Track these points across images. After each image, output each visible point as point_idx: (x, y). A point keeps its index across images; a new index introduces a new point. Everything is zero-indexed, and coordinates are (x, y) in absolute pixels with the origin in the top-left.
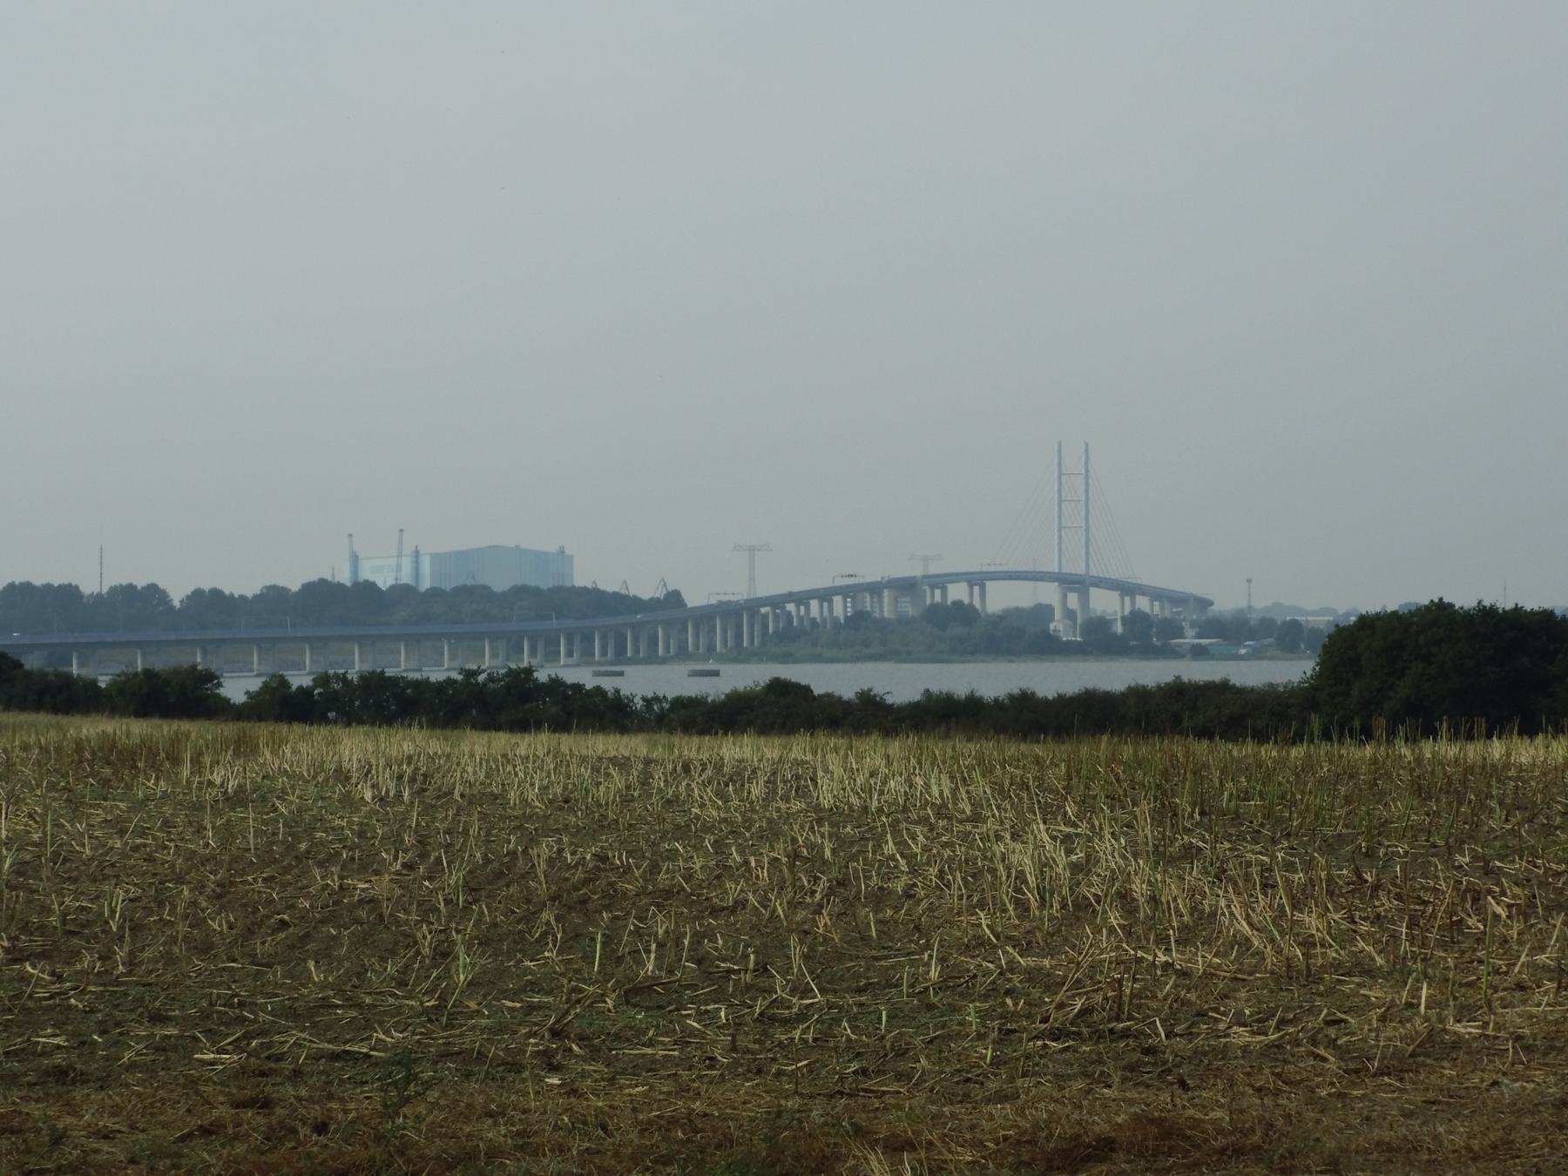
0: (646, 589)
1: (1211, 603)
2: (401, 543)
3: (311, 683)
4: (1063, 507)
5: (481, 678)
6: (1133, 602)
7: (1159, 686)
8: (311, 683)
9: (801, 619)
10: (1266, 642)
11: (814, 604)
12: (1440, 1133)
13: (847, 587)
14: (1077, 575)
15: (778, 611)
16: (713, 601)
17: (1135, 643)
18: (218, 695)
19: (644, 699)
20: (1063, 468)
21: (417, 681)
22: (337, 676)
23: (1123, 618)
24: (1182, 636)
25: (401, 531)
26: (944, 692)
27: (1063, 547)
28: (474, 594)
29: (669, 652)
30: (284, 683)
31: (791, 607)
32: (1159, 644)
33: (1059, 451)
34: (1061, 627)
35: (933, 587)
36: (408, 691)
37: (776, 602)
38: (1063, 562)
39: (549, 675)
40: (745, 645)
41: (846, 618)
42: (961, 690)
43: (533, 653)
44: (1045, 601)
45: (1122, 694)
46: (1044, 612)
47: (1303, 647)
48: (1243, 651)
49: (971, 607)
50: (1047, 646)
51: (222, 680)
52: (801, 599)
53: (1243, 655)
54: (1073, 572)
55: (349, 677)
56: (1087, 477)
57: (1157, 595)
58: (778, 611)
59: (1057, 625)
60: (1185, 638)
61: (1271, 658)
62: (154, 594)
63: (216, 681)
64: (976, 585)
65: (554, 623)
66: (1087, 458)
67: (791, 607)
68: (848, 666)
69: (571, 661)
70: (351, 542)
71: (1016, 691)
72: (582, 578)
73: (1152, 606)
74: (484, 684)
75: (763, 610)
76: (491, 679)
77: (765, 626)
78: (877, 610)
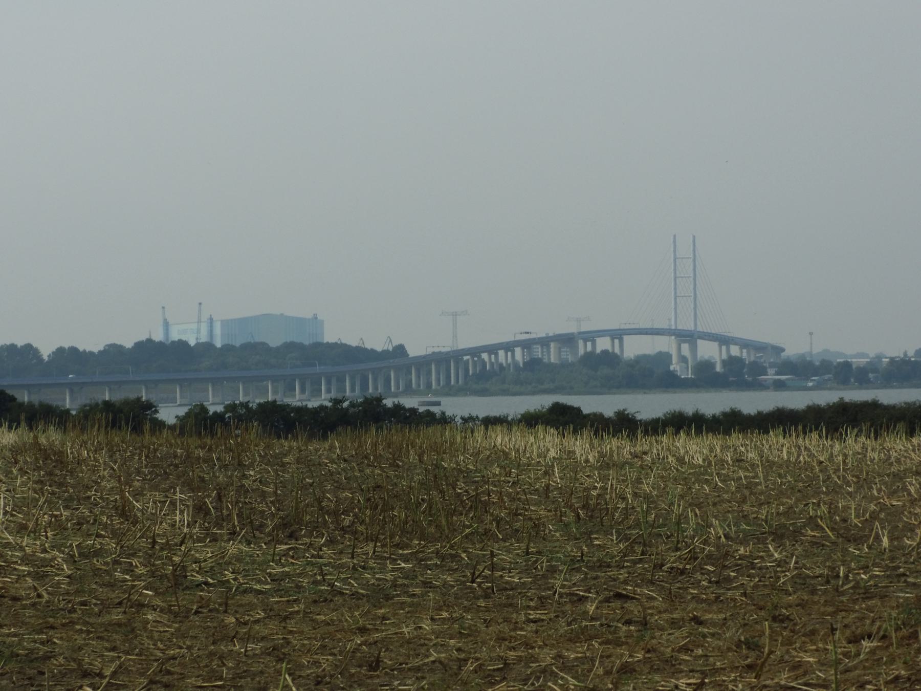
0: (377, 344)
1: (783, 350)
2: (200, 311)
3: (223, 410)
5: (346, 404)
6: (728, 350)
7: (828, 405)
8: (223, 410)
9: (492, 364)
10: (826, 377)
11: (501, 353)
13: (524, 341)
14: (688, 330)
15: (476, 359)
16: (430, 351)
17: (734, 379)
18: (157, 419)
19: (462, 418)
20: (677, 254)
21: (299, 407)
22: (241, 404)
24: (766, 374)
25: (200, 304)
26: (677, 411)
27: (678, 311)
28: (254, 349)
29: (398, 388)
30: (203, 409)
31: (485, 356)
32: (750, 379)
33: (675, 242)
34: (678, 368)
35: (585, 341)
36: (292, 415)
37: (475, 352)
39: (394, 402)
40: (452, 383)
41: (524, 363)
42: (689, 410)
43: (303, 391)
44: (664, 349)
45: (803, 411)
46: (663, 358)
47: (852, 380)
48: (810, 384)
49: (614, 354)
50: (671, 382)
51: (158, 408)
52: (492, 350)
55: (251, 405)
56: (694, 261)
57: (745, 344)
58: (476, 359)
59: (675, 366)
60: (768, 375)
61: (830, 389)
62: (29, 349)
63: (153, 409)
64: (616, 338)
65: (318, 369)
67: (485, 356)
68: (528, 397)
70: (164, 313)
71: (728, 410)
72: (330, 336)
73: (742, 352)
74: (347, 409)
75: (465, 358)
76: (352, 405)
77: (467, 370)
78: (546, 357)
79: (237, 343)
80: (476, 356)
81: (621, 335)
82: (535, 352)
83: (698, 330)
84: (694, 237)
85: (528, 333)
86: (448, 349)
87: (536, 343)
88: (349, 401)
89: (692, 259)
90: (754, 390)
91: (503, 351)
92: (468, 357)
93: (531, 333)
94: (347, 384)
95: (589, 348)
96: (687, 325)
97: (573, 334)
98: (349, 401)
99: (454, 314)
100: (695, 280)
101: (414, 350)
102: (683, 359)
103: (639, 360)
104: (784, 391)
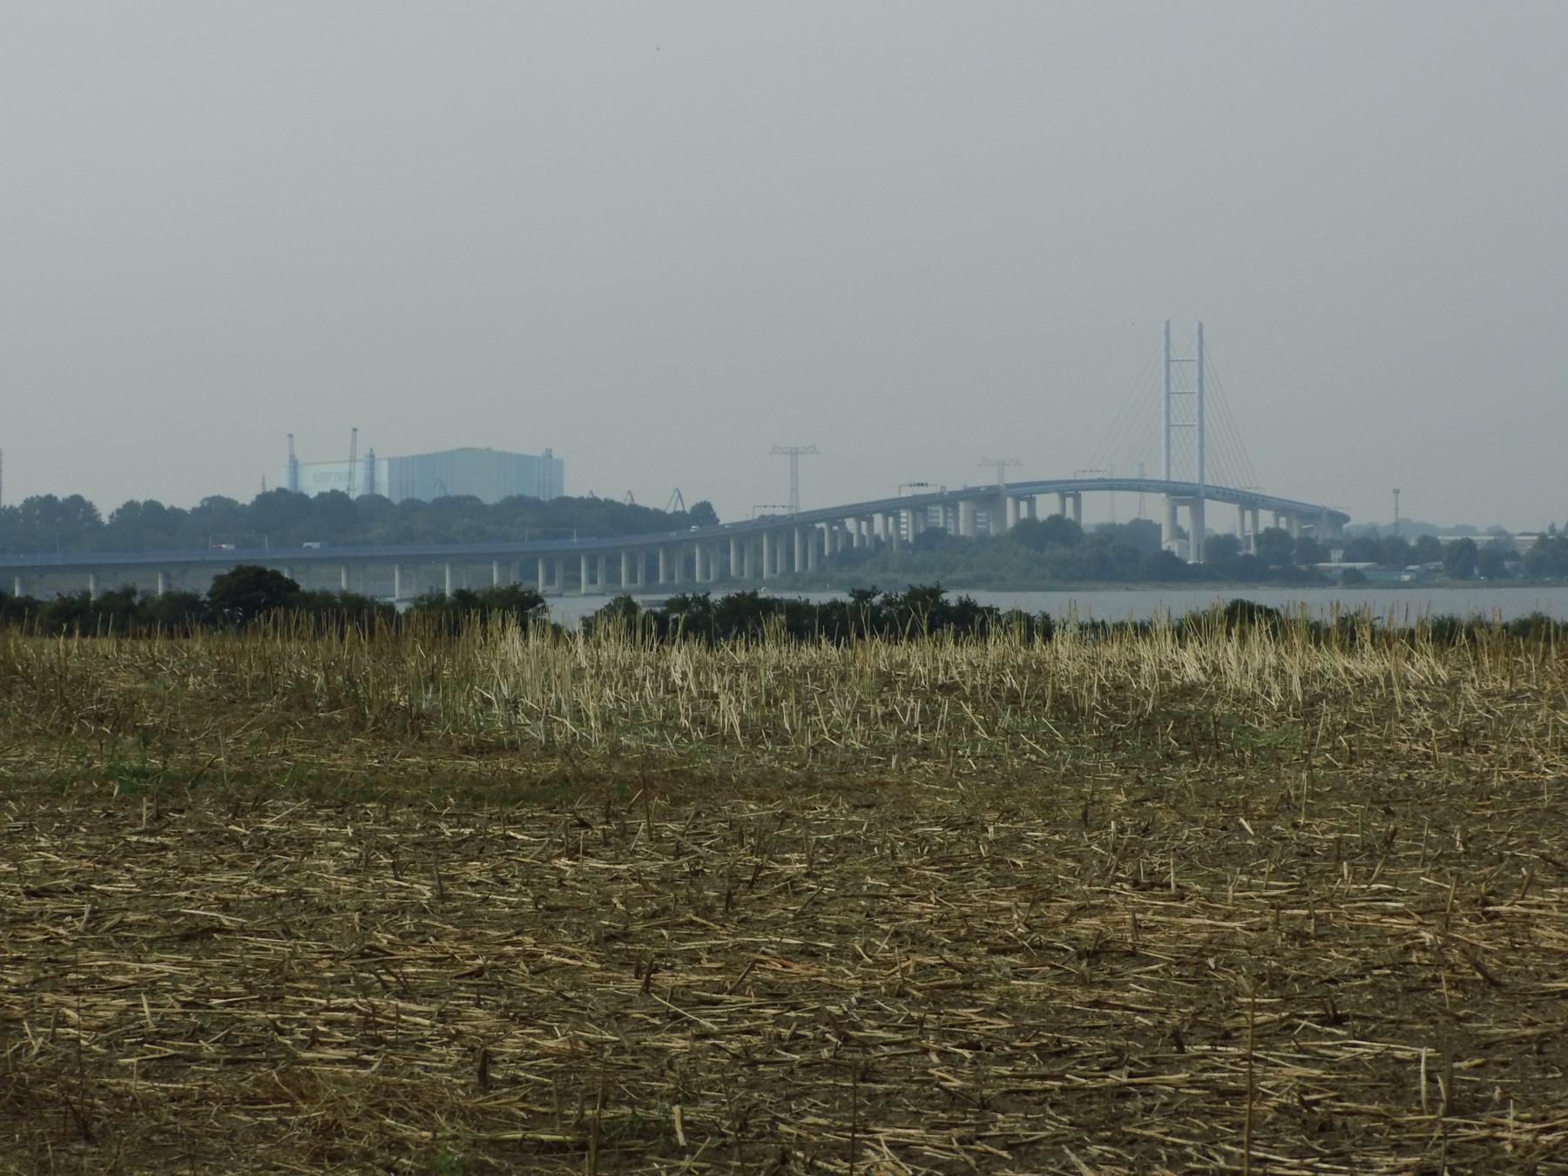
2: (354, 441)
4: (1172, 401)
5: (877, 600)
9: (861, 537)
10: (1432, 566)
11: (878, 519)
12: (682, 1159)
13: (915, 497)
15: (835, 528)
16: (758, 513)
22: (695, 599)
25: (355, 430)
29: (708, 577)
31: (850, 524)
33: (1167, 332)
35: (1018, 499)
37: (835, 517)
38: (1172, 469)
44: (1156, 520)
46: (1144, 530)
47: (1476, 571)
48: (1406, 578)
52: (863, 512)
54: (1184, 480)
58: (835, 528)
59: (1168, 543)
61: (1439, 586)
62: (78, 506)
63: (539, 606)
64: (1069, 496)
66: (1168, 341)
67: (850, 524)
69: (592, 589)
70: (291, 445)
72: (575, 487)
73: (1277, 521)
75: (818, 526)
76: (888, 602)
77: (821, 548)
79: (427, 495)
84: (1201, 326)
87: (936, 503)
92: (823, 525)
94: (623, 568)
95: (1024, 514)
96: (1187, 474)
97: (996, 488)
101: (729, 513)
102: (1179, 533)
103: (1108, 534)
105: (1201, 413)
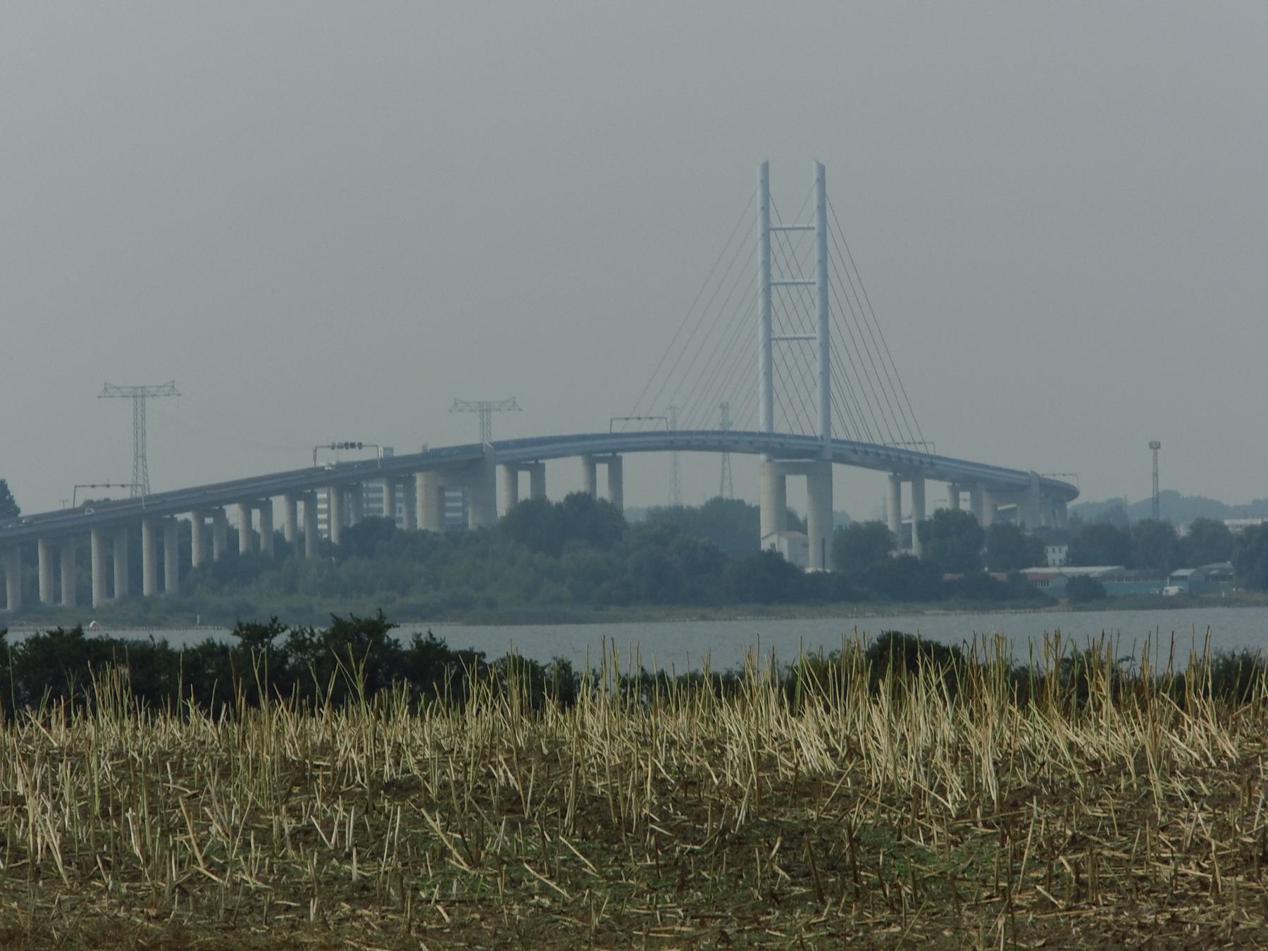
5: (280, 641)
9: (253, 537)
10: (1215, 568)
11: (279, 504)
15: (209, 520)
17: (956, 576)
20: (773, 217)
23: (922, 525)
33: (765, 183)
35: (514, 468)
41: (344, 533)
48: (1173, 590)
53: (1171, 598)
54: (797, 432)
58: (209, 520)
59: (770, 539)
60: (1047, 565)
61: (1228, 603)
64: (602, 460)
73: (956, 500)
75: (180, 517)
76: (298, 644)
77: (185, 554)
78: (403, 515)
80: (210, 514)
81: (614, 452)
82: (370, 501)
83: (833, 436)
84: (822, 169)
85: (353, 446)
86: (125, 494)
87: (376, 475)
88: (288, 632)
89: (816, 232)
90: (1013, 607)
91: (804, 478)
92: (189, 516)
93: (360, 446)
95: (525, 492)
98: (288, 632)
99: (139, 392)
100: (824, 290)
102: (789, 522)
104: (1103, 609)
105: (824, 317)
